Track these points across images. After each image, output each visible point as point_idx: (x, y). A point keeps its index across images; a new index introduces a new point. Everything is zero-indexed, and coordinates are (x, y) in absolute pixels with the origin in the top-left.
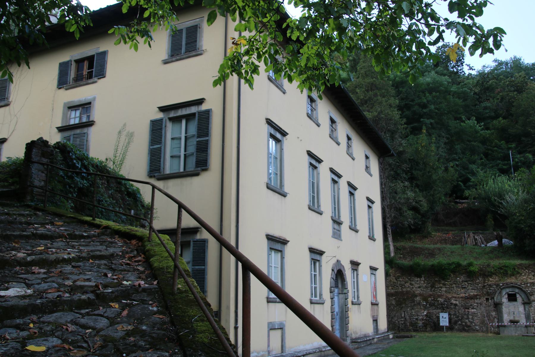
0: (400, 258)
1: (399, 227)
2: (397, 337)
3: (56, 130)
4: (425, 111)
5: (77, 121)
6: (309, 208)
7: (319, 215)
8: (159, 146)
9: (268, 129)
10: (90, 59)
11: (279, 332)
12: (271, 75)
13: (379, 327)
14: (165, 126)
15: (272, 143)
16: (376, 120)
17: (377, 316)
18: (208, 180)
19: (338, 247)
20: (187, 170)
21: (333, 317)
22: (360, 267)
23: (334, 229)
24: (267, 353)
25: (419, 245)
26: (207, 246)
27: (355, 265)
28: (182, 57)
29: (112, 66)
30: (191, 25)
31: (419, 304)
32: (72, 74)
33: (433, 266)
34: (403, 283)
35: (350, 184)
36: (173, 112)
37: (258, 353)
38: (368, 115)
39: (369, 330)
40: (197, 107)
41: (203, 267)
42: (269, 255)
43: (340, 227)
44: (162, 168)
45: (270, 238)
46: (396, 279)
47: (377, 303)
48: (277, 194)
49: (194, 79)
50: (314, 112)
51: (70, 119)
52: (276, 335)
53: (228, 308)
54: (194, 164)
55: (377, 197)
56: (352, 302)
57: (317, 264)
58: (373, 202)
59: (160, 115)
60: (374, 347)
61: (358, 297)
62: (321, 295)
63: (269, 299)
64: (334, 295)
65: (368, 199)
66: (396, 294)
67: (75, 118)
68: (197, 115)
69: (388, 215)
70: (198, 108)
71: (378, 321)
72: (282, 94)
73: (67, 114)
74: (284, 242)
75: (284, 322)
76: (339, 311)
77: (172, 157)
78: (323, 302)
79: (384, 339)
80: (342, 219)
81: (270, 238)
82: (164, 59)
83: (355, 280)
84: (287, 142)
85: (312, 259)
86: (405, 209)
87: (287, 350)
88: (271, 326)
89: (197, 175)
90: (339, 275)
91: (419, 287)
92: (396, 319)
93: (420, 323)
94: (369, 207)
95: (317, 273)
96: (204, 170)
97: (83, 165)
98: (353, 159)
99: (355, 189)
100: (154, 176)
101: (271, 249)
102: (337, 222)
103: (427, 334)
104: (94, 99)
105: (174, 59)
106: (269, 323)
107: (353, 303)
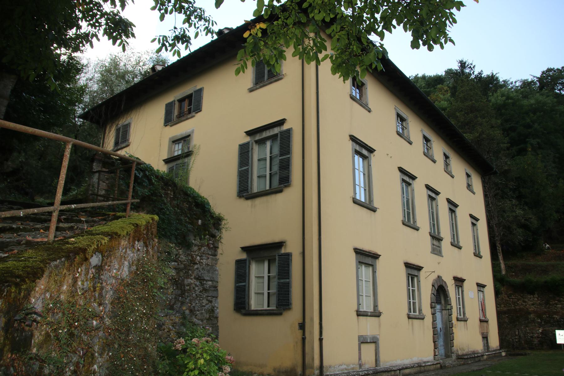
0: (512, 276)
1: (507, 244)
2: (510, 355)
3: (163, 163)
4: (530, 130)
5: (180, 152)
6: (404, 224)
7: (415, 231)
8: (246, 168)
9: (353, 145)
10: (189, 97)
11: (372, 346)
12: (354, 94)
13: (490, 345)
14: (252, 149)
15: (358, 160)
16: (478, 141)
17: (487, 333)
18: (290, 197)
19: (439, 263)
20: (273, 187)
21: (435, 333)
22: (465, 284)
23: (434, 245)
24: (358, 366)
25: (532, 262)
26: (291, 260)
27: (459, 281)
28: (265, 84)
29: (208, 101)
31: (533, 321)
32: (176, 112)
33: (546, 282)
34: (515, 300)
35: (449, 201)
36: (258, 135)
37: (347, 366)
38: (468, 136)
39: (478, 346)
40: (279, 128)
41: (288, 280)
42: (358, 269)
43: (440, 244)
44: (249, 188)
45: (358, 252)
46: (508, 297)
47: (486, 320)
48: (365, 209)
49: (275, 103)
50: (405, 131)
51: (174, 152)
52: (368, 350)
53: (312, 319)
54: (278, 181)
55: (481, 214)
56: (457, 318)
57: (415, 279)
58: (477, 220)
59: (248, 139)
60: (481, 363)
61: (464, 314)
62: (420, 310)
63: (359, 313)
64: (435, 311)
65: (471, 216)
66: (128, 171)
67: (178, 150)
68: (279, 135)
69: (497, 234)
70: (280, 128)
71: (489, 338)
72: (367, 112)
73: (171, 148)
74: (376, 256)
75: (378, 336)
76: (443, 327)
77: (259, 177)
78: (422, 317)
79: (495, 355)
80: (442, 235)
81: (358, 252)
82: (250, 87)
83: (461, 297)
84: (374, 159)
85: (409, 274)
86: (514, 226)
87: (381, 364)
88: (362, 339)
89: (281, 191)
90: (440, 291)
91: (533, 304)
92: (510, 337)
93: (536, 341)
94: (474, 225)
95: (416, 289)
96: (286, 187)
97: (145, 176)
98: (453, 177)
99: (456, 206)
100: (243, 196)
101: (360, 263)
102: (436, 238)
103: (543, 352)
104: (193, 131)
105: (258, 87)
106: (360, 337)
107: (458, 320)
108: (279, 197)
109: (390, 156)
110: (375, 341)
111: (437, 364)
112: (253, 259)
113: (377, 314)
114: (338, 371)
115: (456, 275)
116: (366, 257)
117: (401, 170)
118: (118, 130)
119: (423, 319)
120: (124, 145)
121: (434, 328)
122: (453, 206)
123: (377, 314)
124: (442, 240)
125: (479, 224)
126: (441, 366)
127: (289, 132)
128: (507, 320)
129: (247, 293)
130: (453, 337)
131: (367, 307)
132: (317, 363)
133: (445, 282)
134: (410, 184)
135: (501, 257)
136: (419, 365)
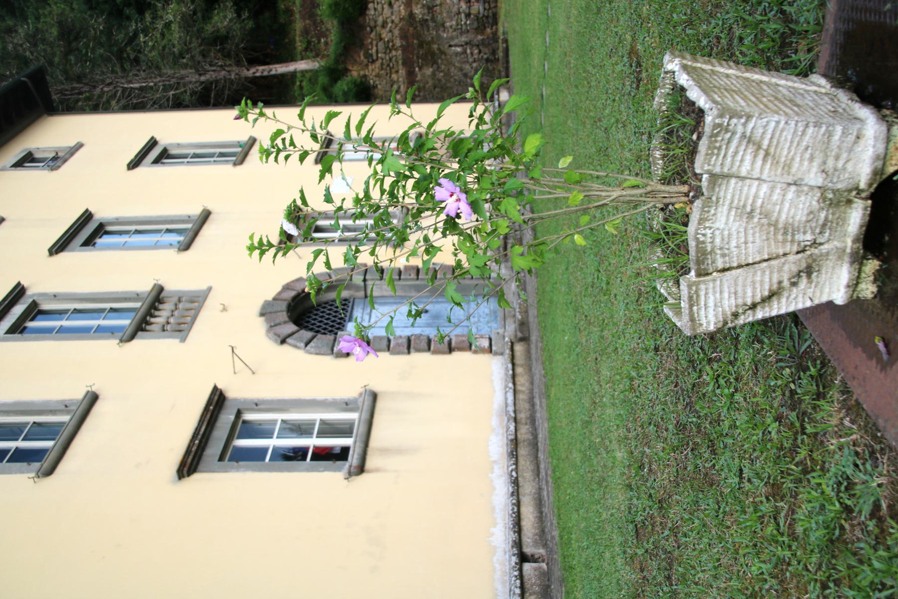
0: (326, 43)
19: (224, 309)
34: (381, 44)
46: (373, 62)
58: (152, 143)
95: (279, 417)
111: (512, 350)
117: (134, 164)
119: (374, 396)
124: (161, 289)
125: (164, 140)
126: (522, 340)
128: (429, 71)
133: (287, 287)
134: (34, 304)
136: (514, 453)
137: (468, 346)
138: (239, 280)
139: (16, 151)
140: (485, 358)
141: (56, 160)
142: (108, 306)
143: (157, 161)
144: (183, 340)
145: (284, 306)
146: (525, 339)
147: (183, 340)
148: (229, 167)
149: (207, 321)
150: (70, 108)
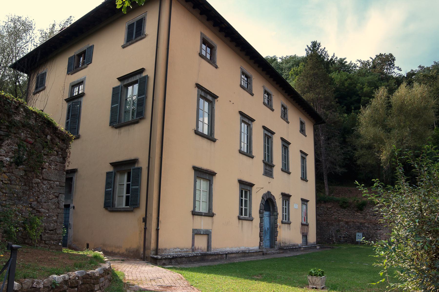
7: (251, 159)
9: (198, 92)
12: (204, 53)
13: (308, 241)
17: (307, 233)
21: (262, 231)
27: (286, 197)
30: (140, 19)
39: (298, 240)
49: (140, 56)
53: (151, 215)
58: (306, 155)
61: (289, 219)
75: (211, 230)
79: (313, 247)
80: (274, 163)
88: (196, 232)
90: (268, 203)
96: (141, 119)
104: (85, 78)
106: (194, 230)
107: (282, 223)
108: (137, 127)
109: (232, 102)
110: (208, 234)
112: (118, 171)
113: (210, 214)
114: (173, 253)
115: (283, 192)
116: (204, 174)
118: (38, 78)
120: (41, 89)
121: (261, 227)
122: (286, 144)
123: (210, 214)
125: (308, 158)
127: (147, 77)
129: (138, 201)
130: (277, 234)
131: (202, 208)
132: (153, 246)
133: (274, 196)
135: (326, 182)
137: (261, 240)
138: (277, 185)
139: (304, 120)
140: (258, 245)
141: (302, 131)
142: (270, 154)
143: (302, 157)
144: (263, 175)
145: (270, 197)
146: (263, 254)
147: (263, 175)
148: (300, 176)
149: (267, 179)
150: (315, 130)
